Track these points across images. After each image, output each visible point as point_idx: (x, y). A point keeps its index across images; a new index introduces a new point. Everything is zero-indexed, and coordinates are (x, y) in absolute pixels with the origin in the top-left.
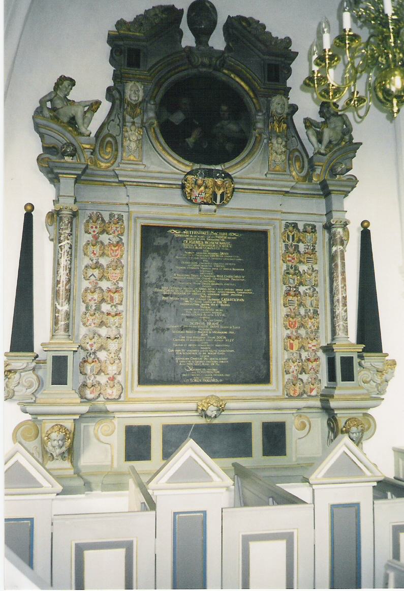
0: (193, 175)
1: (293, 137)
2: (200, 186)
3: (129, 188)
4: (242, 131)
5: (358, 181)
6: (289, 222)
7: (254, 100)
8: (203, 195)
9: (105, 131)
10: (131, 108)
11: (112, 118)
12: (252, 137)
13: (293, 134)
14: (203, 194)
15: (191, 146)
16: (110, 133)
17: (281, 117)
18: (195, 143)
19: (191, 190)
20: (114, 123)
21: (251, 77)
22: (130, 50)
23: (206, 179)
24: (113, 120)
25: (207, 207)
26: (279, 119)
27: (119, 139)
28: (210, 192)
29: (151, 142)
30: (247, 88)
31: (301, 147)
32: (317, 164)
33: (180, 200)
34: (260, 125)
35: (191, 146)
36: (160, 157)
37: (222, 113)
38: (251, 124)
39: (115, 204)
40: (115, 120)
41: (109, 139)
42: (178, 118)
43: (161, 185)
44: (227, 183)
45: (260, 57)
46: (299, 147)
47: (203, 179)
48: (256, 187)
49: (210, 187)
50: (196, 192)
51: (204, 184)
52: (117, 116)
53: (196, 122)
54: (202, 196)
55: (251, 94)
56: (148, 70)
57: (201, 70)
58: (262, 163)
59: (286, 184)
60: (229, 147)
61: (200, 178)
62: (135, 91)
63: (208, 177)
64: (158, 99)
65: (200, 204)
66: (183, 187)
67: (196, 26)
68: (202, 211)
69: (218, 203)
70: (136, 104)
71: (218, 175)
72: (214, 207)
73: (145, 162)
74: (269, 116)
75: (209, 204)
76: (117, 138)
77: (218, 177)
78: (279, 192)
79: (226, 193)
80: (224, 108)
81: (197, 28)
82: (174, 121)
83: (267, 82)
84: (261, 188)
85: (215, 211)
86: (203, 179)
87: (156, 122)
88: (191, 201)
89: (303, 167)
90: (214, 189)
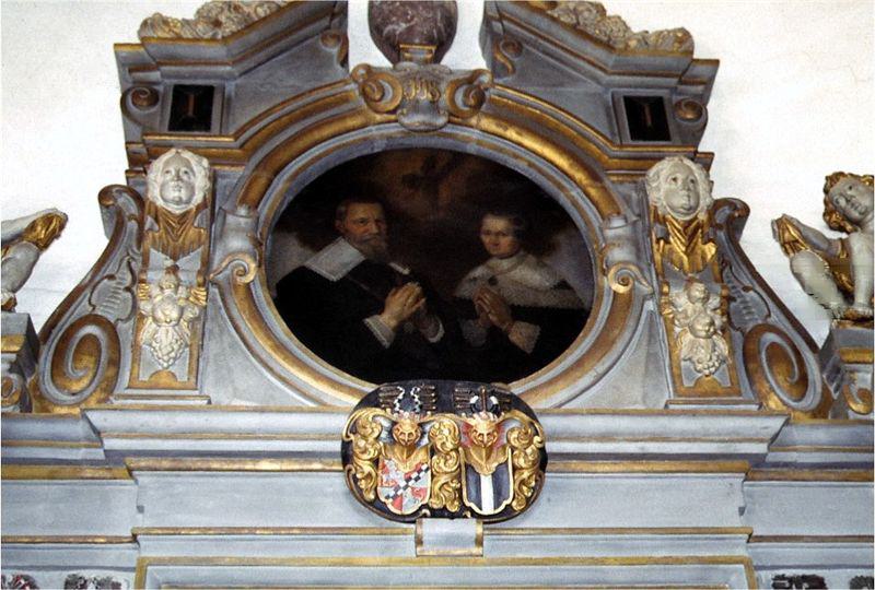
0: (377, 406)
1: (746, 289)
2: (411, 448)
3: (145, 479)
4: (563, 285)
5: (827, 178)
6: (789, 573)
7: (593, 192)
8: (426, 481)
9: (84, 307)
10: (169, 229)
11: (110, 269)
12: (601, 297)
13: (747, 283)
14: (426, 477)
15: (386, 344)
16: (99, 312)
17: (690, 222)
18: (399, 329)
19: (375, 462)
20: (113, 283)
21: (575, 134)
22: (180, 92)
23: (429, 415)
24: (111, 277)
25: (443, 527)
26: (685, 228)
27: (124, 328)
28: (451, 466)
29: (237, 328)
30: (562, 162)
31: (782, 317)
32: (850, 357)
33: (346, 514)
34: (619, 254)
35: (386, 344)
36: (269, 376)
37: (486, 239)
38: (588, 264)
39: (84, 540)
40: (118, 275)
41: (91, 329)
42: (337, 261)
43: (265, 465)
44: (512, 430)
45: (599, 82)
46: (776, 318)
47: (418, 419)
48: (632, 448)
49: (449, 446)
50: (397, 468)
51: (425, 441)
52: (125, 262)
53: (399, 269)
54: (418, 485)
55: (580, 176)
56: (236, 133)
57: (406, 121)
58: (647, 373)
59: (747, 429)
60: (522, 335)
61: (406, 414)
62: (178, 172)
63: (435, 412)
64: (267, 208)
65: (413, 518)
66: (347, 456)
67: (390, 27)
68: (426, 546)
69: (488, 508)
70: (184, 215)
71: (473, 400)
72: (471, 528)
73: (208, 390)
74: (649, 221)
75: (452, 516)
76: (121, 326)
77: (474, 409)
78: (722, 462)
79: (515, 469)
80: (496, 224)
81: (394, 30)
82: (323, 272)
83: (631, 142)
84: (653, 448)
85: (479, 542)
86: (418, 419)
87: (253, 266)
88: (377, 506)
89: (803, 381)
90: (467, 455)
